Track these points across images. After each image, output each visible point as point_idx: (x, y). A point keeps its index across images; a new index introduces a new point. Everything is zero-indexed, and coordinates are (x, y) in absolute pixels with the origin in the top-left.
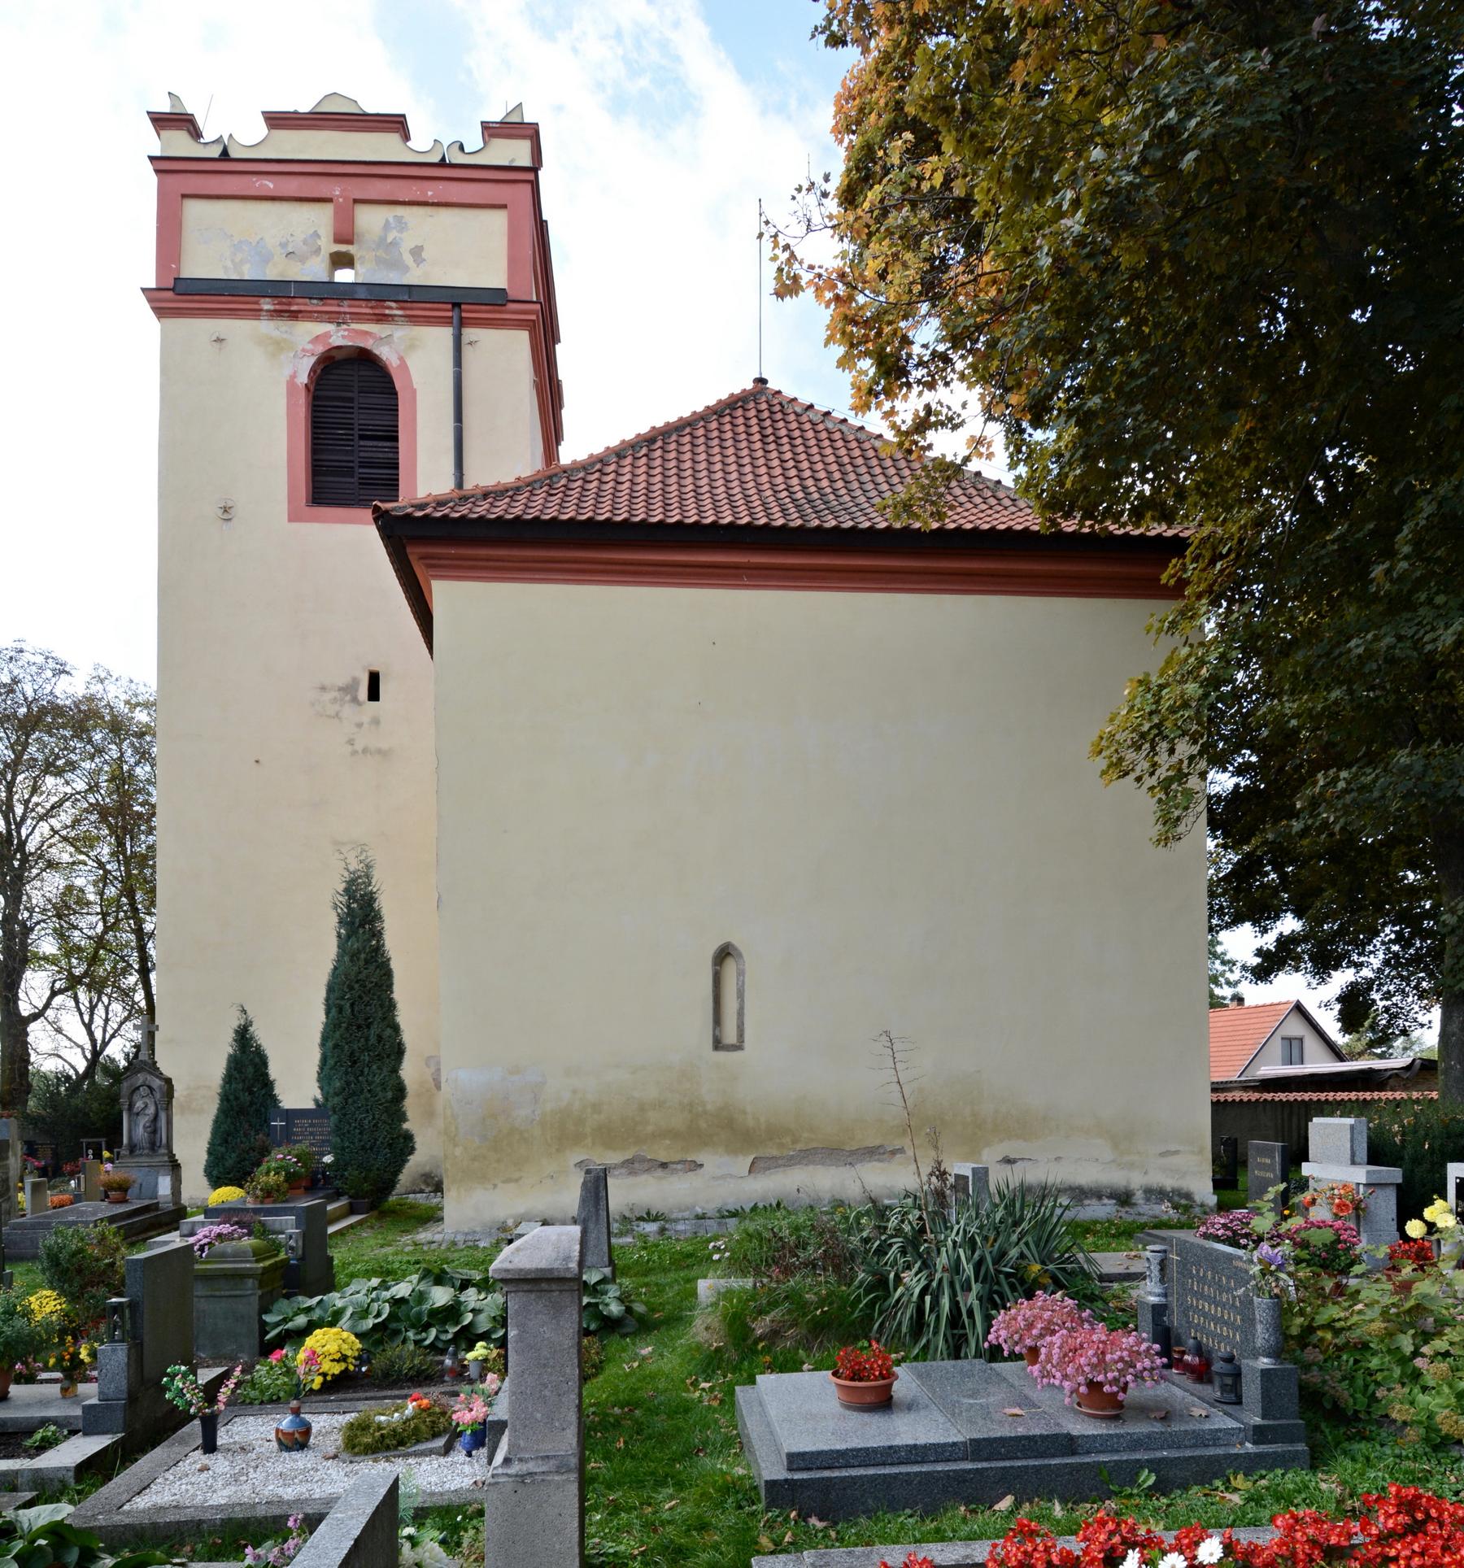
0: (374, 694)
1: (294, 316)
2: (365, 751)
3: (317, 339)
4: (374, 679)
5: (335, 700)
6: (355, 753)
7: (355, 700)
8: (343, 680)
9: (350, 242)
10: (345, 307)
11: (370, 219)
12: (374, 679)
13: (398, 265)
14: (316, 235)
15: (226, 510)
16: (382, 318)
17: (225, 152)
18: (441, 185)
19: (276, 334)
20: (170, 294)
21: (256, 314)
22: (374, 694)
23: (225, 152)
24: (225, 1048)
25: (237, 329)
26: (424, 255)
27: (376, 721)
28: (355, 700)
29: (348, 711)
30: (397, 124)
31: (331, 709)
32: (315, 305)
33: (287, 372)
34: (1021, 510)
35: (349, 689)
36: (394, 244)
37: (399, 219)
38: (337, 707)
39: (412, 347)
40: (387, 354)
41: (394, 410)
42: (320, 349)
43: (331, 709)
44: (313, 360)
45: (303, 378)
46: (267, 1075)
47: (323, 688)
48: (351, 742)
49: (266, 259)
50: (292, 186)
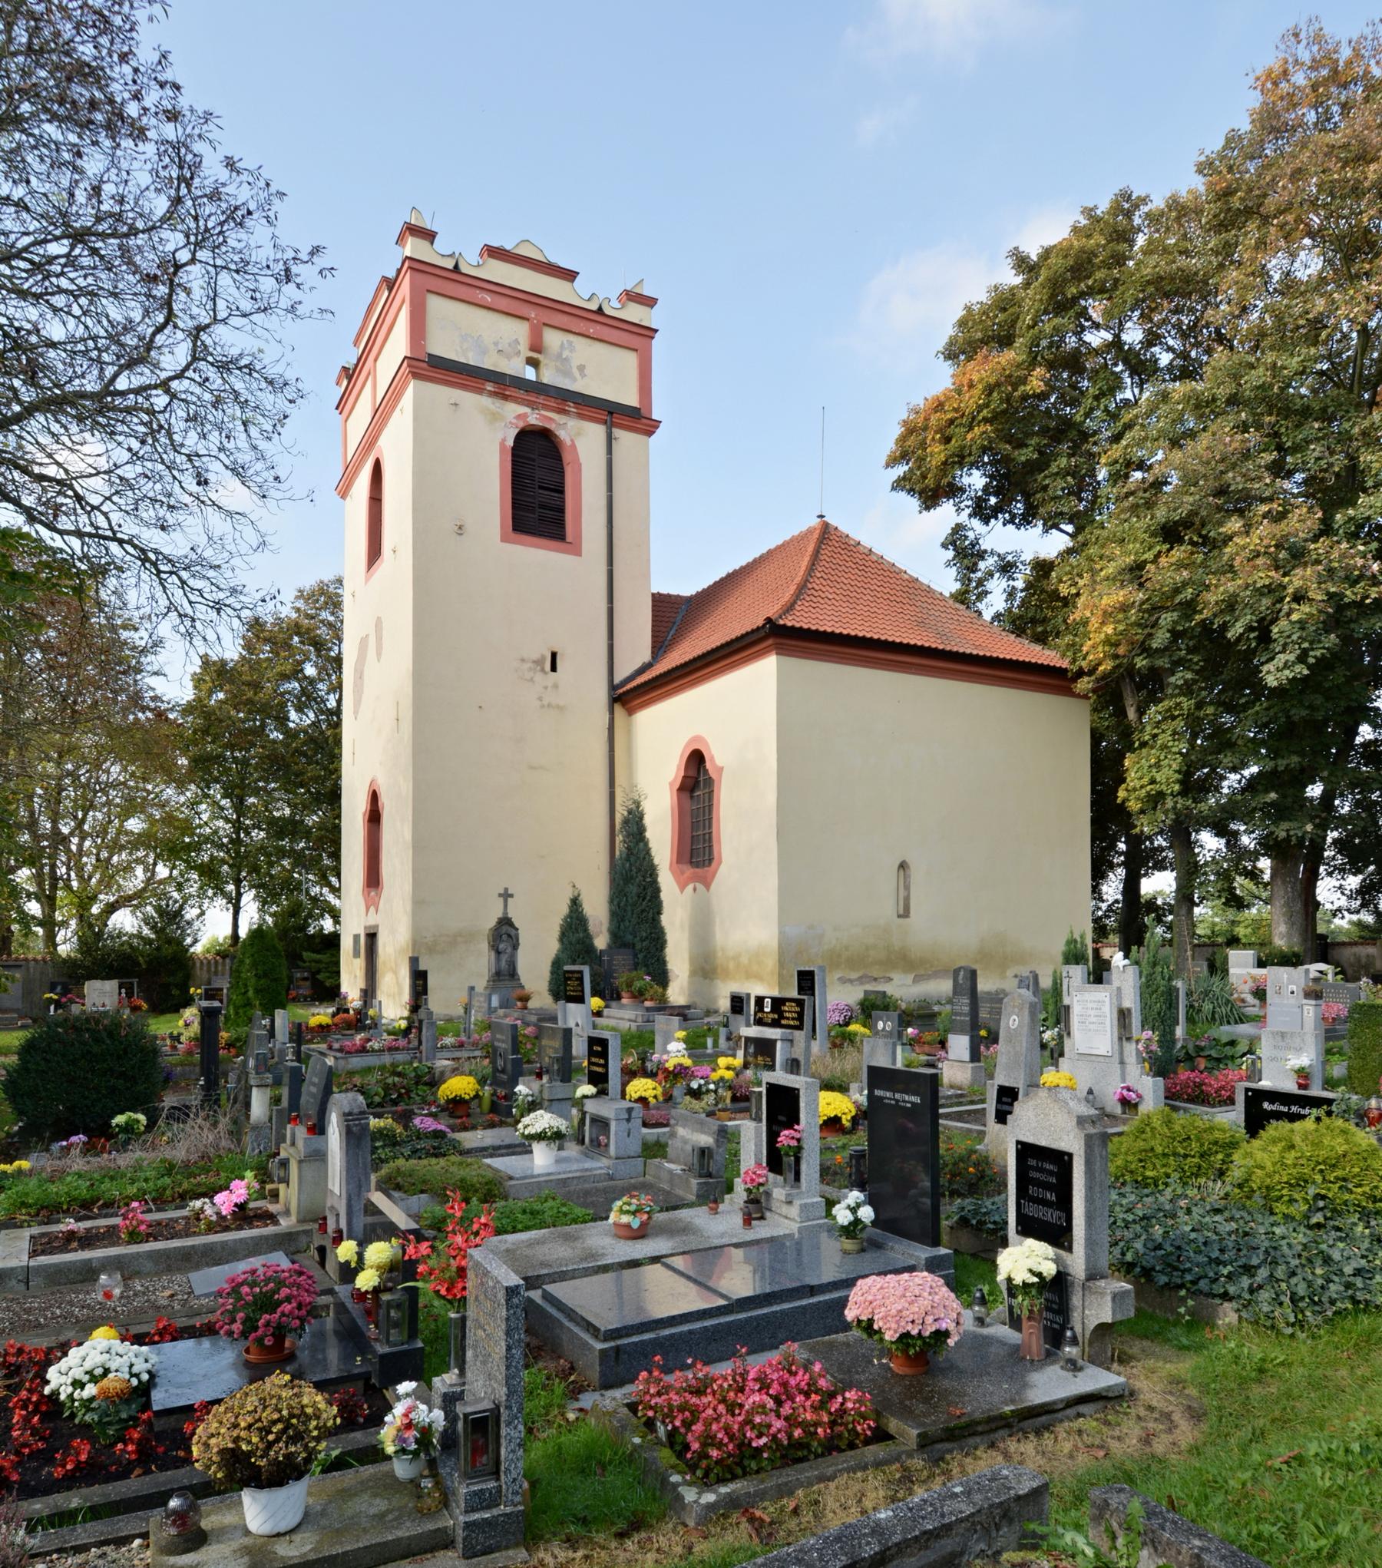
0: (554, 668)
1: (506, 398)
2: (549, 705)
3: (519, 417)
4: (554, 655)
5: (530, 669)
6: (543, 706)
7: (543, 670)
8: (536, 656)
9: (539, 351)
10: (541, 400)
11: (553, 339)
12: (554, 655)
13: (567, 373)
14: (517, 342)
15: (460, 528)
16: (562, 411)
17: (456, 266)
18: (599, 327)
19: (492, 407)
20: (425, 365)
21: (480, 391)
22: (554, 668)
23: (456, 266)
24: (564, 909)
25: (471, 401)
26: (586, 372)
27: (556, 686)
28: (543, 670)
29: (538, 677)
30: (570, 275)
31: (528, 675)
32: (521, 394)
33: (500, 436)
34: (20, 437)
35: (539, 662)
36: (566, 359)
37: (570, 343)
38: (531, 674)
39: (579, 434)
40: (563, 434)
41: (561, 472)
42: (521, 424)
43: (528, 675)
44: (516, 431)
45: (510, 443)
46: (659, 921)
47: (523, 660)
48: (540, 699)
49: (484, 352)
50: (503, 303)
